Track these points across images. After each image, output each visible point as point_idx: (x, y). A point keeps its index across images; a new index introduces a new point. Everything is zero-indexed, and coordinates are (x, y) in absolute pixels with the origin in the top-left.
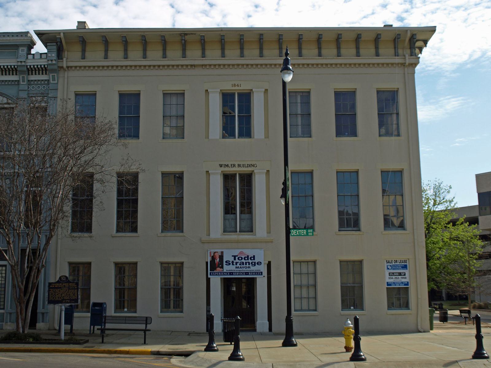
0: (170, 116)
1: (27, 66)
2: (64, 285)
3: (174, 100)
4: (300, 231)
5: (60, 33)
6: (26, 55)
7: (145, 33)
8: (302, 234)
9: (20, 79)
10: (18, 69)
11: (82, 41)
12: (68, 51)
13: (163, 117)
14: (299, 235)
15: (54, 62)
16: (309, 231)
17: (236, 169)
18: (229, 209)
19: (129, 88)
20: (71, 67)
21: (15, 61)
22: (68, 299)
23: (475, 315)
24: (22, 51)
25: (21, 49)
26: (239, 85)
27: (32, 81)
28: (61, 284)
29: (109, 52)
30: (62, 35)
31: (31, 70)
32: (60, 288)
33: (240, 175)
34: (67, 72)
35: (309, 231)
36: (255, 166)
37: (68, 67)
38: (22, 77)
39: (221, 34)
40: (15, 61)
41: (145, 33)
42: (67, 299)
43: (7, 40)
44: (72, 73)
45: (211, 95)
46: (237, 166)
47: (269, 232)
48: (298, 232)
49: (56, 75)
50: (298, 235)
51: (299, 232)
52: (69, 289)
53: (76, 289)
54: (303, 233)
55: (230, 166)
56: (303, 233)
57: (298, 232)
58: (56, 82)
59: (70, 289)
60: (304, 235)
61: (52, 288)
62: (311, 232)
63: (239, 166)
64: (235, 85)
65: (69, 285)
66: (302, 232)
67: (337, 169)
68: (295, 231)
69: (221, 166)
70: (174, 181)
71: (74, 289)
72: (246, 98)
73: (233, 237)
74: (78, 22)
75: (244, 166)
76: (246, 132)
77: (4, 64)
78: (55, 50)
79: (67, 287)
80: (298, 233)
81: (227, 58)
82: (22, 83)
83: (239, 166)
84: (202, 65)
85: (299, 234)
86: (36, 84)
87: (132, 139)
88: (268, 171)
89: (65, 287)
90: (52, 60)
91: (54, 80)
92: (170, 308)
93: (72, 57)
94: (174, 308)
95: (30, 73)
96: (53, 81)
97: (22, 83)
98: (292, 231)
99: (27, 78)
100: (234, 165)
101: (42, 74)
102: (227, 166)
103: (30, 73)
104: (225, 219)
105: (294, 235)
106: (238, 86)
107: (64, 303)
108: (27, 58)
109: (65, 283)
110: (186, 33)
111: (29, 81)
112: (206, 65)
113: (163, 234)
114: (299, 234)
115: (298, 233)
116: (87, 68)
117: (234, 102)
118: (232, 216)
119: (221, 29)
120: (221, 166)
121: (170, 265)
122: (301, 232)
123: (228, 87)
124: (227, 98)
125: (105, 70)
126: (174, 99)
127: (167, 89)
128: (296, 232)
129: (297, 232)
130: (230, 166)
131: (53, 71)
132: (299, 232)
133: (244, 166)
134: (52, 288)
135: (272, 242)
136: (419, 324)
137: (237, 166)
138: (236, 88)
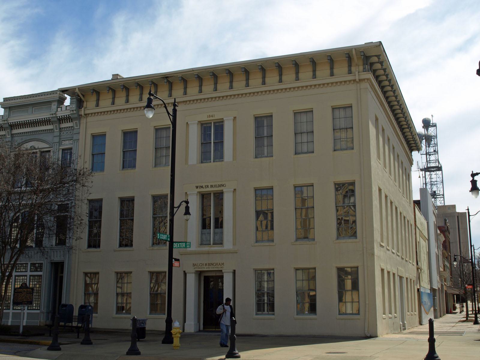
0: (301, 133)
1: (9, 123)
2: (24, 290)
3: (342, 113)
4: (180, 244)
5: (76, 88)
6: (56, 108)
7: (136, 81)
8: (182, 247)
9: (6, 133)
10: (52, 120)
11: (277, 66)
12: (87, 102)
13: (295, 134)
14: (180, 248)
15: (75, 112)
16: (187, 244)
17: (209, 189)
18: (205, 225)
19: (129, 127)
20: (89, 114)
21: (49, 114)
22: (26, 301)
23: (133, 317)
24: (54, 106)
25: (53, 104)
26: (213, 116)
27: (63, 128)
28: (22, 289)
29: (233, 83)
30: (77, 89)
31: (61, 120)
32: (21, 292)
33: (214, 194)
34: (86, 118)
35: (187, 244)
36: (225, 186)
37: (360, 80)
38: (55, 126)
39: (275, 62)
40: (49, 114)
41: (136, 81)
42: (25, 301)
43: (43, 98)
44: (90, 119)
45: (190, 126)
46: (209, 186)
47: (234, 244)
48: (179, 245)
49: (78, 121)
50: (178, 248)
51: (180, 244)
52: (27, 293)
53: (32, 293)
54: (182, 246)
55: (204, 187)
56: (182, 246)
57: (179, 245)
58: (78, 127)
59: (28, 293)
60: (183, 248)
61: (16, 292)
62: (189, 245)
63: (212, 186)
64: (210, 116)
65: (27, 290)
66: (182, 245)
67: (294, 184)
68: (177, 244)
69: (197, 187)
70: (127, 205)
71: (31, 293)
72: (219, 126)
73: (206, 249)
74: (113, 75)
75: (215, 186)
76: (220, 157)
77: (33, 119)
78: (75, 102)
79: (26, 292)
80: (179, 246)
81: (336, 77)
82: (56, 131)
83: (212, 186)
84: (184, 102)
85: (180, 246)
86: (65, 131)
87: (127, 169)
88: (235, 190)
89: (24, 292)
90: (73, 111)
91: (77, 126)
92: (264, 311)
93: (90, 105)
94: (267, 311)
95: (61, 122)
96: (76, 127)
97: (56, 131)
98: (174, 244)
99: (59, 126)
100: (208, 186)
101: (70, 122)
102: (202, 187)
103: (61, 122)
104: (202, 234)
105: (175, 248)
106: (212, 117)
107: (23, 304)
108: (57, 110)
109: (25, 289)
110: (166, 76)
111: (12, 134)
112: (186, 101)
113: (338, 241)
114: (180, 246)
115: (179, 246)
116: (292, 90)
117: (211, 132)
118: (208, 230)
119: (192, 70)
120: (197, 187)
121: (263, 271)
122: (181, 244)
123: (204, 118)
124: (205, 127)
125: (260, 95)
126: (303, 115)
127: (158, 125)
128: (177, 244)
129: (178, 245)
130: (204, 187)
131: (76, 119)
132: (180, 244)
133: (215, 186)
134: (16, 292)
135: (237, 253)
136: (366, 329)
137: (209, 186)
138: (211, 118)
